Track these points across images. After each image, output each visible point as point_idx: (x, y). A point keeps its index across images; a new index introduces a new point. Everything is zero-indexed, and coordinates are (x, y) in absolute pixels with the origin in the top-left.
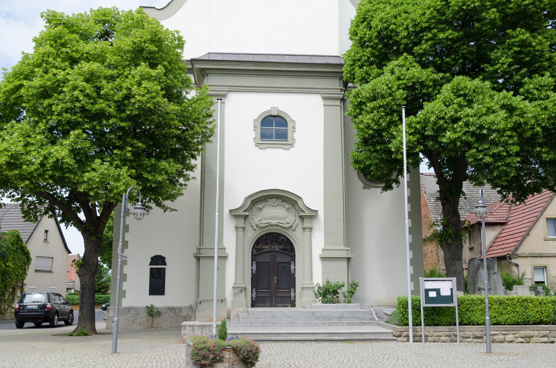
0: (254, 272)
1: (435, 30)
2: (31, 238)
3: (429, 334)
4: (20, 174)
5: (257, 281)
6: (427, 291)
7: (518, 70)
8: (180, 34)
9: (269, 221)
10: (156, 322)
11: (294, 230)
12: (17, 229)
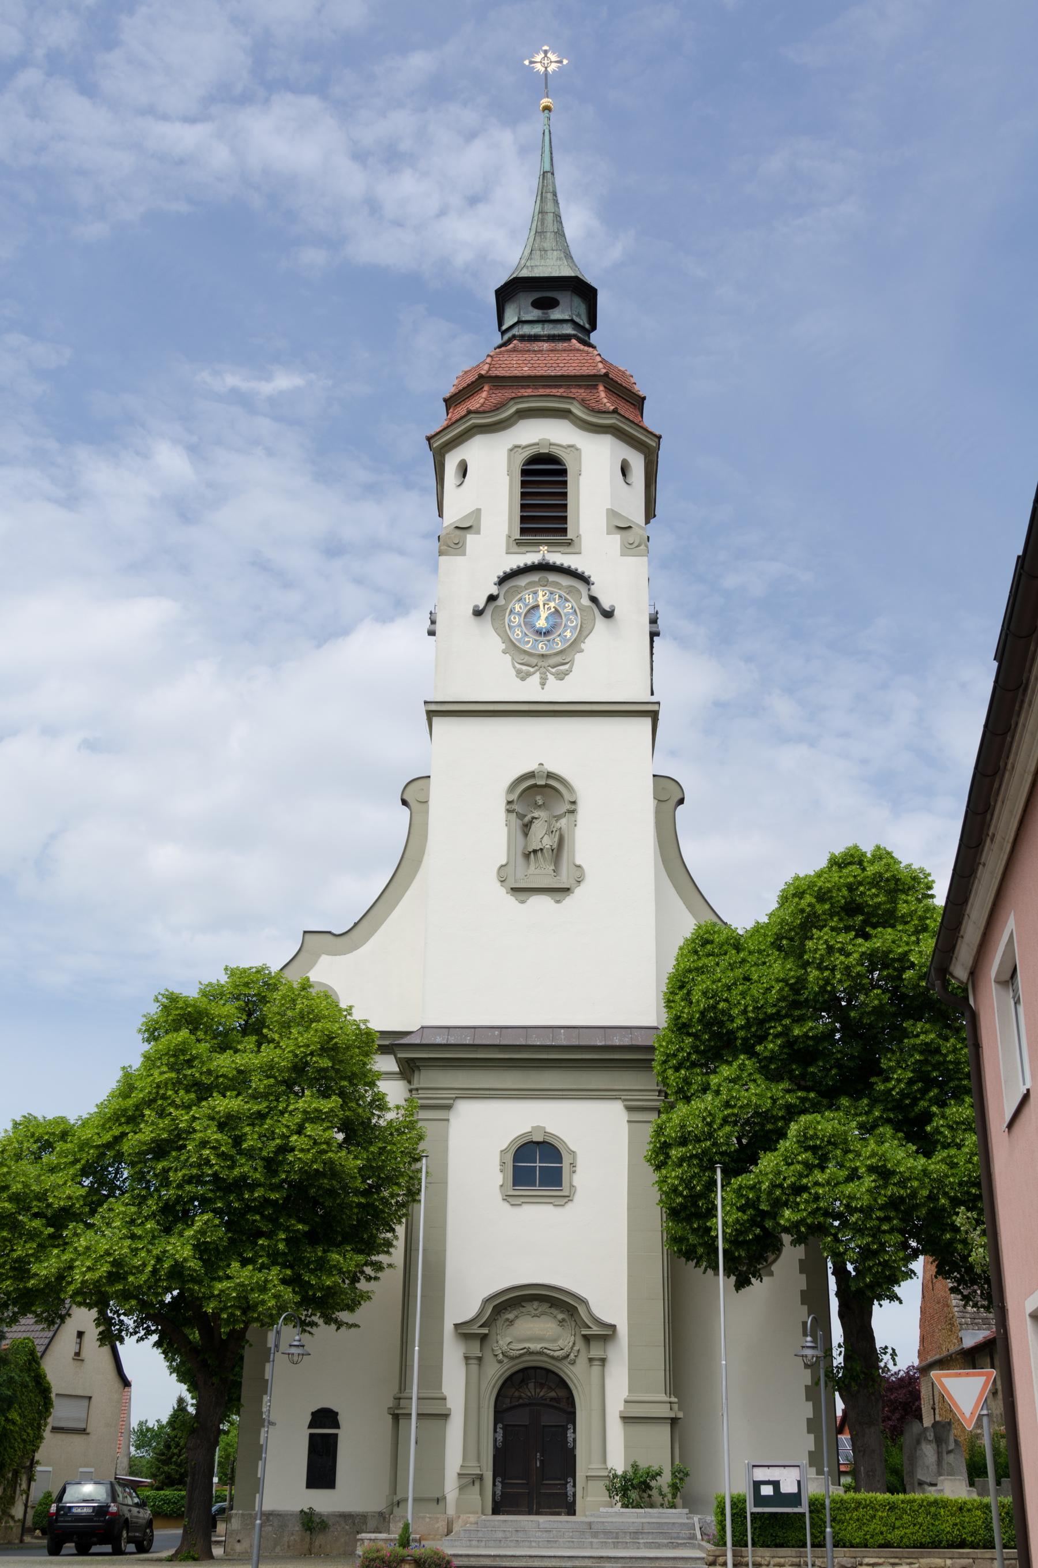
0: (499, 1444)
1: (787, 1021)
2: (48, 1352)
3: (763, 1562)
4: (124, 1290)
5: (504, 1461)
6: (757, 1485)
7: (924, 1091)
8: (369, 1025)
9: (527, 1345)
10: (317, 1543)
11: (573, 1363)
12: (31, 1335)
